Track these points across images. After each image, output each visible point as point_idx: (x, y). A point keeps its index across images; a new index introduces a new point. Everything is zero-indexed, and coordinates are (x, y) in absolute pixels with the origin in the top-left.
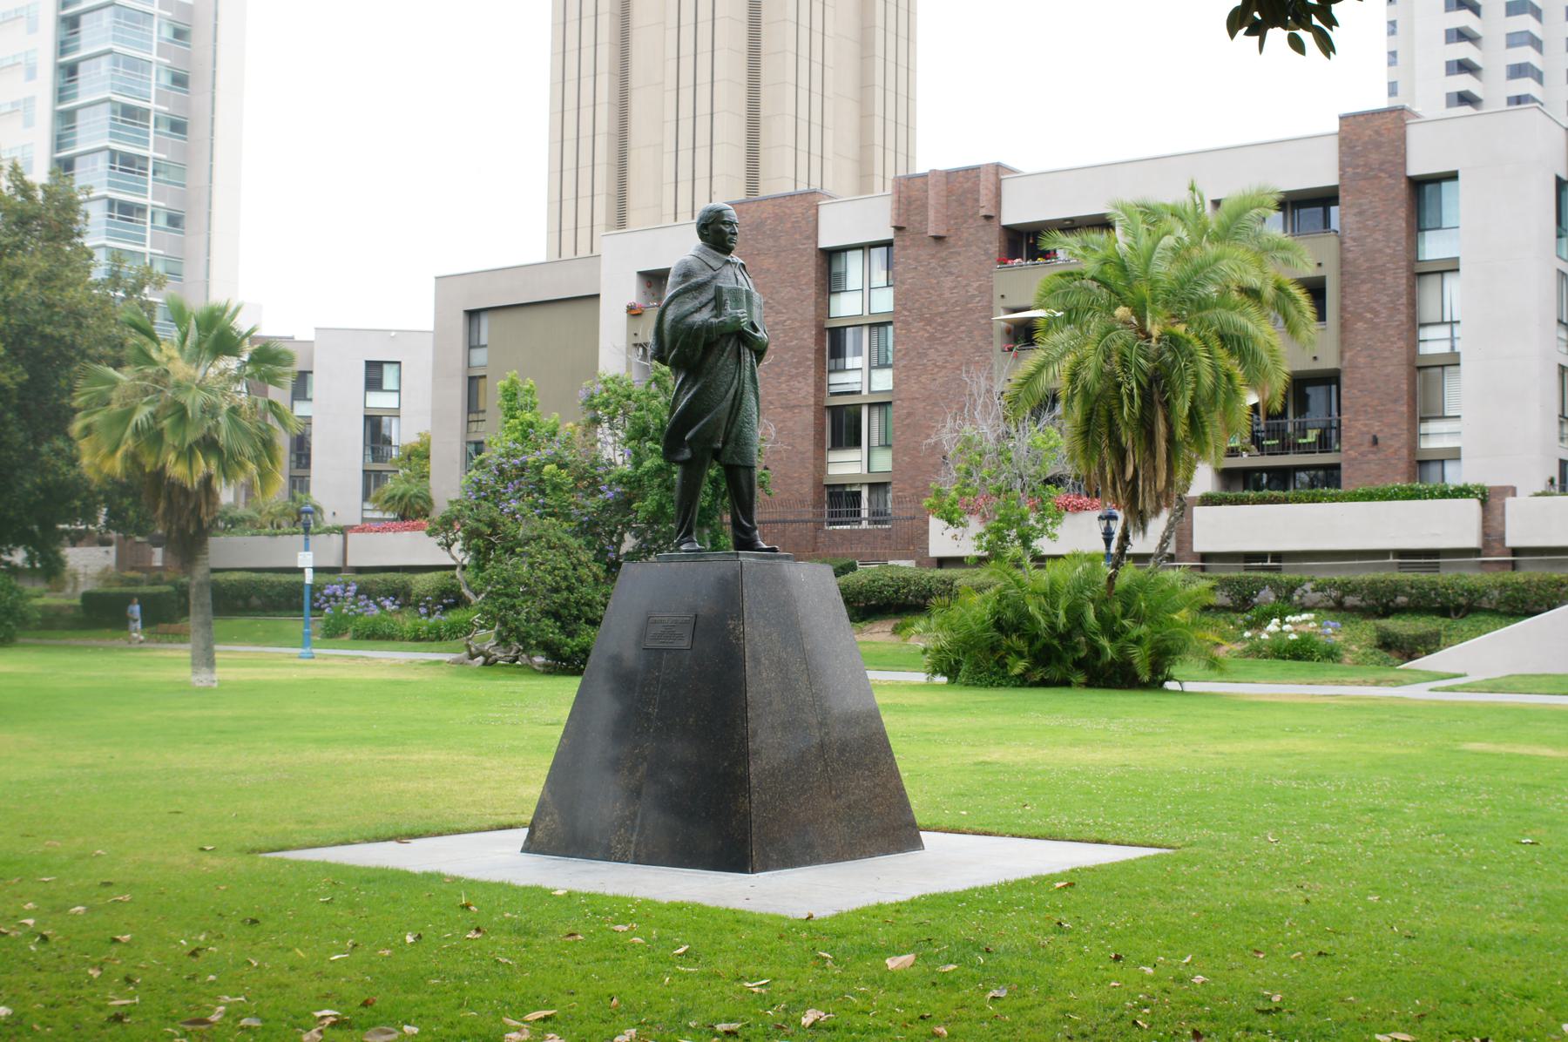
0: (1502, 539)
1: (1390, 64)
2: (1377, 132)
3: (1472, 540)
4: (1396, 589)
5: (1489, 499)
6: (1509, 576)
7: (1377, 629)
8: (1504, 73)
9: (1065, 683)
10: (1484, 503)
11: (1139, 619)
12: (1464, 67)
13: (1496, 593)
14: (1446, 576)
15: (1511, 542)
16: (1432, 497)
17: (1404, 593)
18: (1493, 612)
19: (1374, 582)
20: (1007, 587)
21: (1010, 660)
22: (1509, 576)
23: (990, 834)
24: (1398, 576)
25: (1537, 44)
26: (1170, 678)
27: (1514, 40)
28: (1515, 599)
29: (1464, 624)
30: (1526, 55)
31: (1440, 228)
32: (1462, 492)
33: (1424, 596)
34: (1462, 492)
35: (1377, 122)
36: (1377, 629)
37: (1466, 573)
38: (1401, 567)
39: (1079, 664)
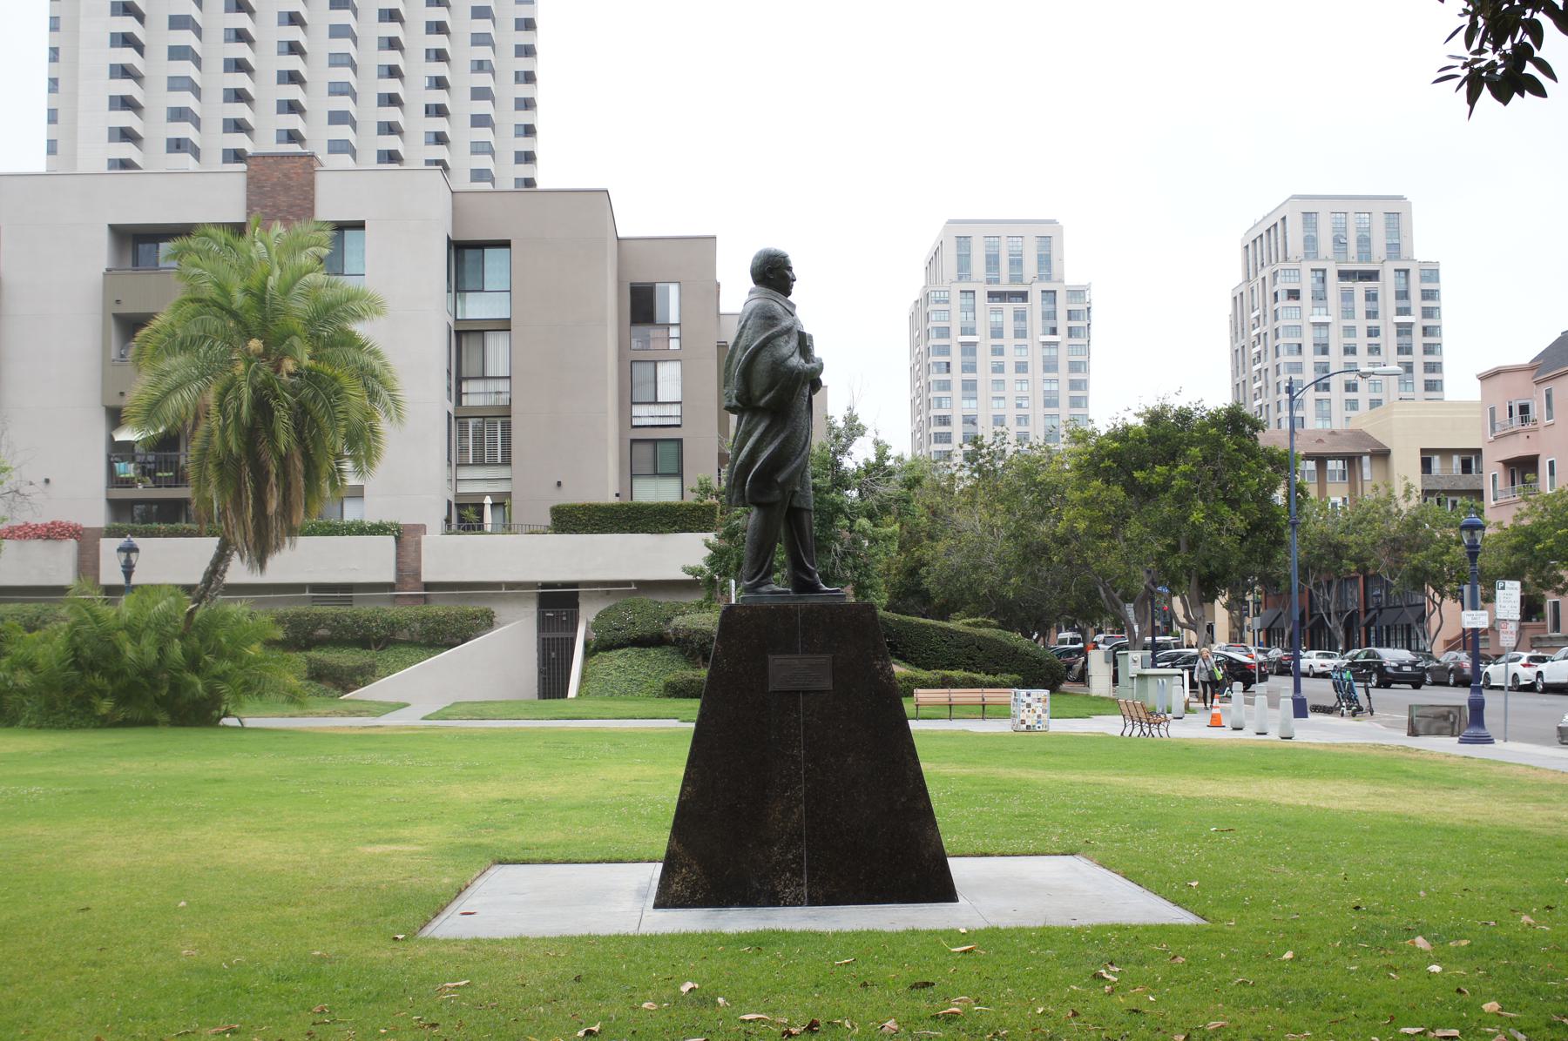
0: (418, 574)
1: (50, 91)
2: (285, 175)
3: (389, 576)
4: (319, 621)
5: (405, 537)
6: (423, 610)
7: (310, 660)
8: (164, 114)
9: (149, 723)
10: (398, 539)
11: (220, 654)
12: (127, 103)
13: (418, 625)
14: (363, 608)
15: (426, 577)
16: (350, 533)
17: (327, 626)
18: (411, 643)
19: (298, 615)
20: (82, 622)
21: (95, 700)
22: (423, 610)
23: (986, 855)
24: (320, 609)
25: (197, 91)
26: (227, 715)
27: (176, 84)
28: (436, 632)
29: (389, 655)
30: (186, 99)
31: (482, 291)
32: (379, 529)
33: (346, 628)
34: (379, 529)
35: (286, 166)
36: (310, 660)
37: (382, 606)
38: (314, 600)
39: (161, 702)
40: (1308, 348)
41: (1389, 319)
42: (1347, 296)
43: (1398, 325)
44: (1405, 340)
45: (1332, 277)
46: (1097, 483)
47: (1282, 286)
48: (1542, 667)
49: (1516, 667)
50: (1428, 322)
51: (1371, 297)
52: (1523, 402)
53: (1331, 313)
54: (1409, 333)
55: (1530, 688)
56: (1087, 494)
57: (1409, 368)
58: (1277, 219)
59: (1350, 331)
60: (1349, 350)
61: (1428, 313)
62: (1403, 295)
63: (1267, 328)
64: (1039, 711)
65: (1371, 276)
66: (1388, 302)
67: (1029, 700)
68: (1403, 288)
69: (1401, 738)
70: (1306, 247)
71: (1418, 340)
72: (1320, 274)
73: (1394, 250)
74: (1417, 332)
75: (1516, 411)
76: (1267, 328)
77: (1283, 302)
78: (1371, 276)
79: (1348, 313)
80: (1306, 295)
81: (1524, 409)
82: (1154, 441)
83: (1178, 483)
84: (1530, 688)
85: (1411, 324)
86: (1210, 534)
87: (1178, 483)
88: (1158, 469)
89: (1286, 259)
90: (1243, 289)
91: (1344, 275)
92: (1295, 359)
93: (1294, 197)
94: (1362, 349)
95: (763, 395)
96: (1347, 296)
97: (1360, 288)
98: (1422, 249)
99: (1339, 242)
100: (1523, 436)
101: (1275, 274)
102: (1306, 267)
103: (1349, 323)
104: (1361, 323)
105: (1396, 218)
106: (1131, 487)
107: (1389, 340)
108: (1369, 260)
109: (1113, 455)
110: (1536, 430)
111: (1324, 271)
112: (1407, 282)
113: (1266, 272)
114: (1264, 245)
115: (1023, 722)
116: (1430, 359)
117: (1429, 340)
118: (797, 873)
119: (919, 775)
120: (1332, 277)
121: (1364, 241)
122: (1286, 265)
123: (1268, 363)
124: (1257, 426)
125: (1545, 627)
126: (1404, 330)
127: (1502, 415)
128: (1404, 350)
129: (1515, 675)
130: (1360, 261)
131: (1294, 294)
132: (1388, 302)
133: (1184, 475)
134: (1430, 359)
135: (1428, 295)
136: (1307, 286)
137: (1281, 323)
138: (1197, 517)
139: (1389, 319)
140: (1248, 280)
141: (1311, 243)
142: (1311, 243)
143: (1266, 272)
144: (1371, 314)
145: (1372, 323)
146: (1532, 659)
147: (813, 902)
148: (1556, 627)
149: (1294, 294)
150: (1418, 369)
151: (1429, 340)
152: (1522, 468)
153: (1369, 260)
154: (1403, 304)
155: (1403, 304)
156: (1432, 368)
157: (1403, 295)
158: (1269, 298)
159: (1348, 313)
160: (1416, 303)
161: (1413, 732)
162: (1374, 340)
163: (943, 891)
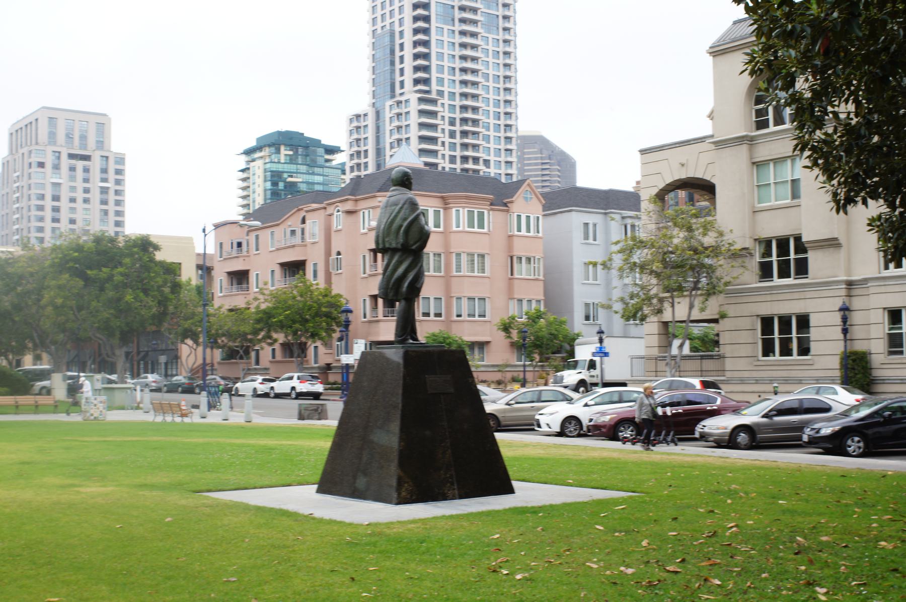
40: (48, 197)
41: (96, 184)
42: (72, 169)
43: (101, 188)
44: (104, 196)
45: (64, 157)
46: (67, 276)
47: (35, 159)
48: (272, 384)
49: (256, 385)
50: (118, 188)
51: (86, 170)
52: (239, 240)
53: (63, 178)
54: (107, 193)
55: (266, 395)
56: (60, 282)
57: (106, 213)
58: (32, 119)
59: (73, 189)
60: (73, 200)
61: (118, 182)
62: (104, 171)
63: (24, 183)
64: (101, 409)
65: (87, 158)
66: (96, 174)
67: (95, 402)
68: (104, 167)
69: (295, 422)
70: (49, 138)
71: (112, 197)
72: (57, 154)
73: (100, 145)
74: (111, 192)
75: (235, 245)
76: (24, 183)
77: (35, 169)
78: (87, 158)
79: (73, 178)
80: (49, 166)
81: (239, 245)
82: (99, 253)
83: (117, 278)
84: (266, 395)
85: (108, 188)
86: (136, 308)
87: (117, 278)
88: (104, 269)
89: (37, 143)
90: (9, 158)
91: (72, 156)
92: (40, 203)
93: (44, 108)
94: (80, 200)
95: (415, 243)
96: (72, 169)
97: (80, 164)
98: (116, 145)
99: (69, 137)
100: (241, 259)
101: (30, 152)
102: (50, 149)
103: (73, 184)
104: (80, 185)
105: (102, 126)
106: (87, 279)
107: (95, 196)
108: (85, 149)
109: (76, 260)
110: (248, 256)
111: (59, 152)
112: (107, 164)
113: (25, 150)
114: (23, 134)
115: (92, 415)
116: (118, 208)
117: (118, 198)
118: (452, 484)
119: (401, 439)
120: (64, 157)
121: (83, 138)
122: (37, 147)
123: (24, 203)
124: (157, 248)
125: (250, 363)
126: (104, 191)
127: (227, 247)
128: (104, 202)
129: (255, 389)
130: (81, 149)
131: (41, 165)
132: (96, 174)
133: (121, 274)
134: (118, 208)
135: (119, 172)
136: (49, 160)
137: (32, 181)
138: (129, 298)
139: (96, 184)
140: (11, 152)
141: (52, 135)
142: (52, 135)
143: (25, 150)
144: (86, 180)
145: (87, 185)
146: (264, 380)
147: (461, 497)
148: (257, 363)
149: (41, 165)
150: (111, 214)
151: (118, 198)
152: (240, 277)
153: (85, 149)
154: (104, 176)
155: (104, 176)
156: (119, 213)
157: (104, 171)
158: (26, 166)
159: (73, 178)
160: (112, 176)
161: (301, 417)
162: (87, 196)
163: (510, 490)
